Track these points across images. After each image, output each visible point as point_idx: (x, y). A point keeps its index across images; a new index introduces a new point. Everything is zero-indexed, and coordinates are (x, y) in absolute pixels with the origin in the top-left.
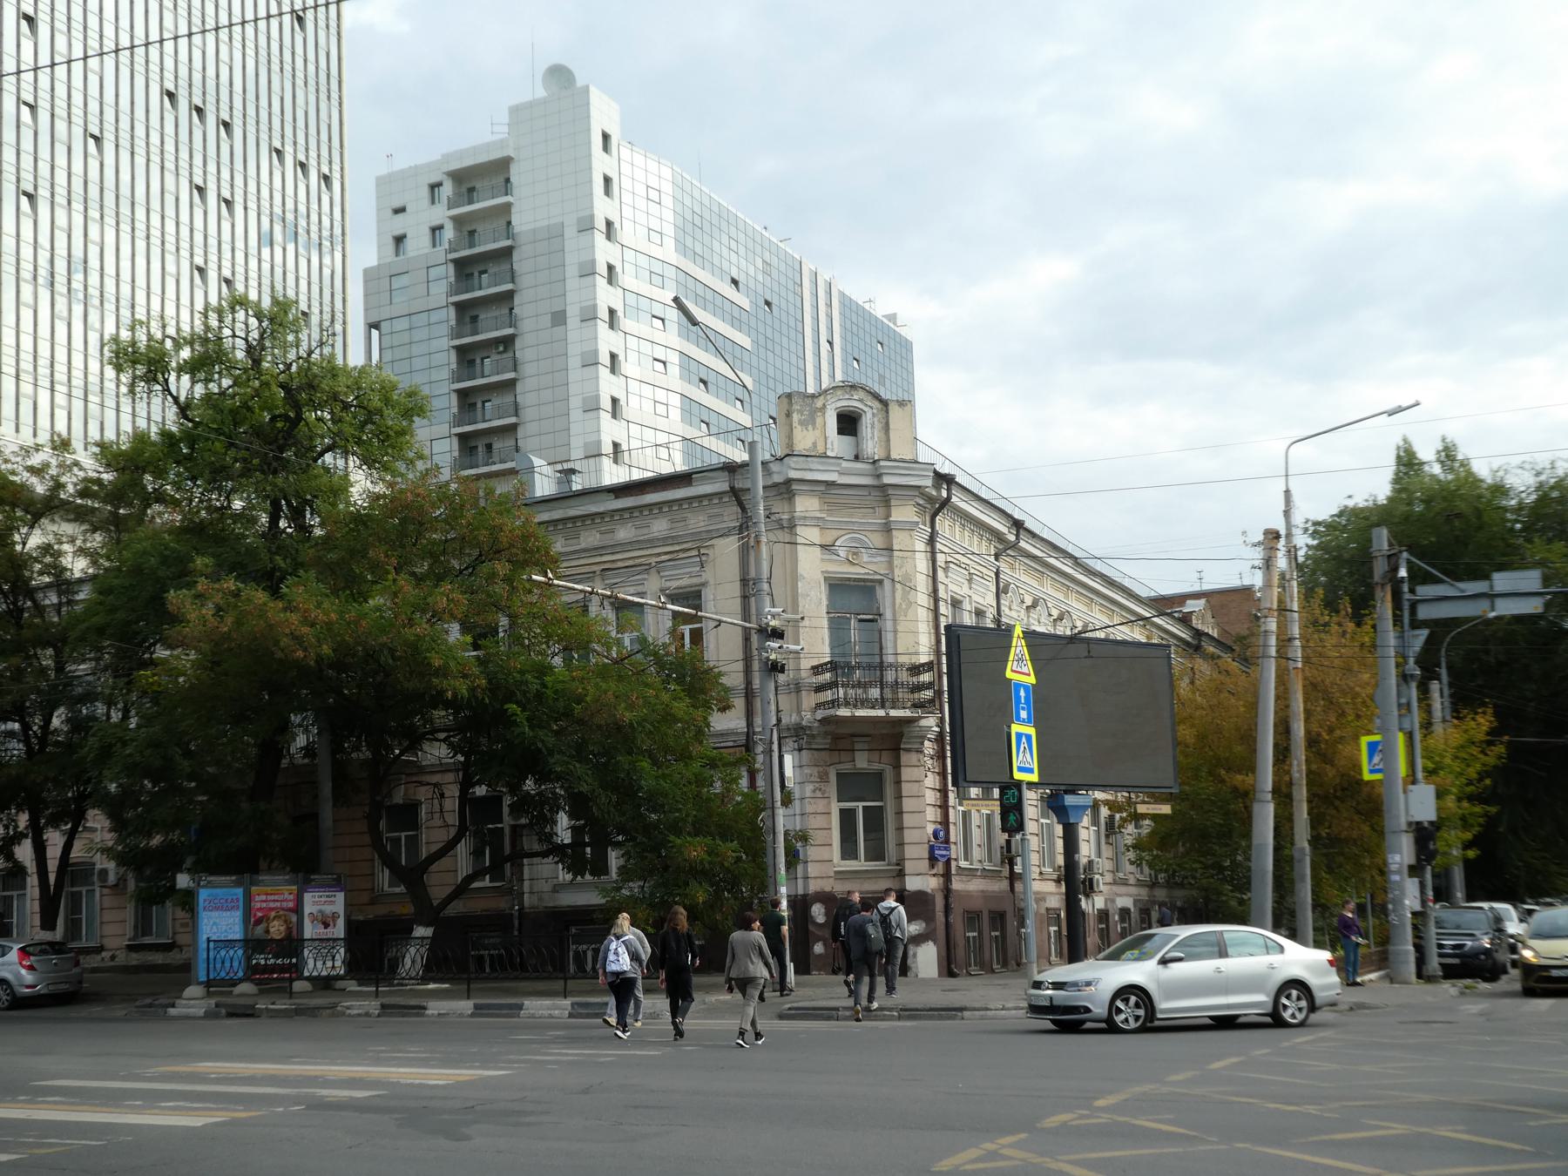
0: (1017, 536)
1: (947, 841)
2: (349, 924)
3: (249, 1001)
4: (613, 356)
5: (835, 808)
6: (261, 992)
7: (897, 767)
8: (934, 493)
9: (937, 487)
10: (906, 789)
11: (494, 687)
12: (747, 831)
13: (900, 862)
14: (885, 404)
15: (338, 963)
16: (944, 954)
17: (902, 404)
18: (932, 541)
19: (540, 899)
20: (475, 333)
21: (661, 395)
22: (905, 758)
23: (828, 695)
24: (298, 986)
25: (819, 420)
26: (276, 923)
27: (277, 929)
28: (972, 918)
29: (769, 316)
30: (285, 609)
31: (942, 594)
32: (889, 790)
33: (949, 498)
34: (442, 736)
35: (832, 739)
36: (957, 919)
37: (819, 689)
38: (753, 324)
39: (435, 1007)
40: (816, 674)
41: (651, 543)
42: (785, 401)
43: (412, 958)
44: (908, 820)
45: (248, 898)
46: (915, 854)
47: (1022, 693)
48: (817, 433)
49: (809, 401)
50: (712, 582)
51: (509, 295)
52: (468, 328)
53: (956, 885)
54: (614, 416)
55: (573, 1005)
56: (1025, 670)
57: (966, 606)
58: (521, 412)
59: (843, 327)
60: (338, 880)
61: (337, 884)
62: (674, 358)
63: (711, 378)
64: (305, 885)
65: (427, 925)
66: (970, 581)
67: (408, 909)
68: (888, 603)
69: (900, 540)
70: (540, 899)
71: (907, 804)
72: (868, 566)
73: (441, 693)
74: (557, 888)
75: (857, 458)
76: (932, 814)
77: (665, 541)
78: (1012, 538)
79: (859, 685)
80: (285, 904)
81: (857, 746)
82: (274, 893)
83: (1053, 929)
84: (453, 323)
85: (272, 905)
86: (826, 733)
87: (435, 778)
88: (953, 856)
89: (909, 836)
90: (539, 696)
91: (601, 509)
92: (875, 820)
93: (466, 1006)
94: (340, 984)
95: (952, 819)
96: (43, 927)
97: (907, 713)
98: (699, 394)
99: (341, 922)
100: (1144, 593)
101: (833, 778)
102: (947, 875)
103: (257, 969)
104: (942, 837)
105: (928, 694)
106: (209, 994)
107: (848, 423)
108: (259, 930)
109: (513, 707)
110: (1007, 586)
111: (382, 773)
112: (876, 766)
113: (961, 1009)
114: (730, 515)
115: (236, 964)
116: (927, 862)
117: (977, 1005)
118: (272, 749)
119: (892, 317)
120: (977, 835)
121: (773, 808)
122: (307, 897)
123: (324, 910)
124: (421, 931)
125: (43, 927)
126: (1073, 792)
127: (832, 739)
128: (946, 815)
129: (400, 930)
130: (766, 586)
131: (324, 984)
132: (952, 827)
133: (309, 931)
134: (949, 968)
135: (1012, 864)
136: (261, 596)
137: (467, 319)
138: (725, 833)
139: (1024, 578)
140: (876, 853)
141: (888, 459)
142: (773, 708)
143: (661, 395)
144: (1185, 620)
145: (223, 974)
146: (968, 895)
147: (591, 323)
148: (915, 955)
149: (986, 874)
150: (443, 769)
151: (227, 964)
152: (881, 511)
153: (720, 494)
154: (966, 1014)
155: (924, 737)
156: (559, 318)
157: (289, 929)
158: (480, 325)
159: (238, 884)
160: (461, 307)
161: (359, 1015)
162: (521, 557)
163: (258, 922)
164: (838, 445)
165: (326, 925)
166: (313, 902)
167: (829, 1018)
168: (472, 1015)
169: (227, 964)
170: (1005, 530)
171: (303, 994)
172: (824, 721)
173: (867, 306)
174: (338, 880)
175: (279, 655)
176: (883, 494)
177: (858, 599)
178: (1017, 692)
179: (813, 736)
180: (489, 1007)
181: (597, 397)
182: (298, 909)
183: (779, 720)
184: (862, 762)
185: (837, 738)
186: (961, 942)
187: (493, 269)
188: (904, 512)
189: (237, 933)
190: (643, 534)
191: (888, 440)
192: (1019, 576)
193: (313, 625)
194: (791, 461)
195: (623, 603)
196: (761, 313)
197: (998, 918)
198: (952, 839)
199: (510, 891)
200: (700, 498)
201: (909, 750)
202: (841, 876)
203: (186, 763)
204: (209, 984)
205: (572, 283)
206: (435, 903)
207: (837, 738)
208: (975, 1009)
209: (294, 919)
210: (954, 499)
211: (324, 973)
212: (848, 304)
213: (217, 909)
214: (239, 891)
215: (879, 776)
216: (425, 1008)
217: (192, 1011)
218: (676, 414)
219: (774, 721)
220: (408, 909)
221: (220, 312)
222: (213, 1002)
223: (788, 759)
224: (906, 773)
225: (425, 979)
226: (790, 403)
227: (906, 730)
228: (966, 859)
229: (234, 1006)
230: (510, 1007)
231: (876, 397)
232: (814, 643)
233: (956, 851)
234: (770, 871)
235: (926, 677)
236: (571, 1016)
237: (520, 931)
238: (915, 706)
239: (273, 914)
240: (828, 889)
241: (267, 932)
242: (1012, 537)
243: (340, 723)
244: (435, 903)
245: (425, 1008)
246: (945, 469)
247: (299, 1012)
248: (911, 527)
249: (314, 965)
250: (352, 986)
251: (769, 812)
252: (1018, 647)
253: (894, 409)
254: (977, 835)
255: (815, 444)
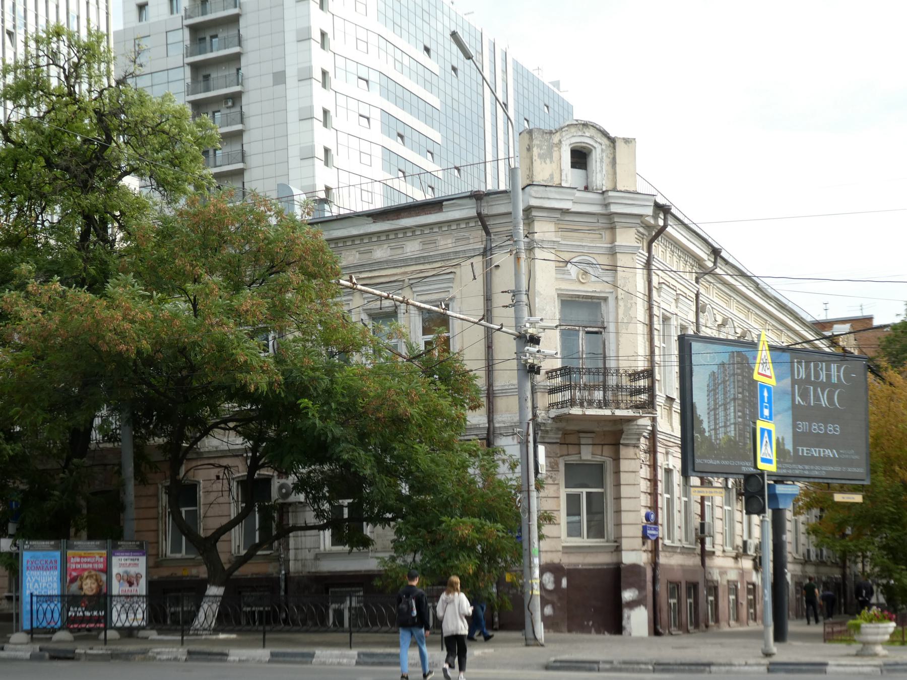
0: (715, 263)
1: (656, 523)
2: (151, 584)
3: (69, 647)
4: (326, 112)
5: (563, 492)
6: (76, 639)
7: (617, 459)
8: (652, 222)
9: (655, 217)
10: (624, 478)
11: (289, 384)
12: (505, 513)
13: (618, 540)
14: (613, 141)
15: (140, 616)
16: (652, 617)
17: (627, 141)
18: (648, 265)
19: (304, 566)
20: (207, 89)
21: (365, 147)
22: (623, 452)
23: (558, 397)
24: (112, 634)
25: (555, 155)
26: (88, 581)
27: (89, 587)
28: (674, 587)
29: (455, 80)
30: (108, 308)
31: (656, 311)
32: (609, 479)
33: (665, 226)
34: (231, 425)
35: (566, 434)
36: (662, 588)
37: (552, 391)
38: (442, 86)
39: (236, 654)
40: (549, 378)
41: (405, 262)
42: (526, 136)
43: (207, 612)
44: (625, 504)
45: (65, 560)
46: (631, 532)
47: (766, 394)
48: (554, 165)
49: (547, 137)
50: (458, 296)
51: (237, 57)
52: (201, 85)
53: (663, 560)
54: (326, 163)
55: (359, 655)
56: (768, 373)
57: (674, 322)
58: (247, 159)
59: (516, 91)
60: (141, 546)
61: (140, 549)
62: (375, 115)
63: (407, 133)
64: (114, 550)
65: (219, 585)
66: (677, 300)
67: (202, 572)
68: (612, 318)
69: (622, 260)
70: (304, 566)
71: (625, 491)
72: (592, 287)
73: (244, 386)
74: (318, 557)
75: (586, 188)
76: (645, 500)
77: (418, 261)
78: (710, 264)
79: (586, 387)
80: (96, 566)
81: (583, 441)
82: (86, 555)
83: (732, 597)
84: (189, 80)
85: (85, 566)
86: (558, 429)
87: (225, 462)
88: (660, 536)
89: (625, 518)
90: (328, 392)
91: (362, 232)
92: (596, 506)
93: (263, 654)
94: (142, 633)
95: (660, 505)
96: (570, 534)
97: (630, 413)
98: (396, 146)
99: (143, 582)
100: (809, 319)
101: (562, 468)
102: (655, 552)
103: (74, 620)
104: (652, 520)
105: (644, 397)
106: (33, 640)
107: (580, 158)
108: (74, 588)
109: (305, 402)
110: (705, 306)
111: (177, 455)
112: (599, 459)
113: (709, 665)
114: (476, 239)
115: (56, 615)
116: (640, 541)
117: (721, 661)
118: (80, 436)
119: (557, 84)
120: (678, 519)
121: (529, 491)
122: (115, 560)
123: (128, 570)
124: (214, 591)
125: (570, 534)
126: (782, 482)
127: (566, 434)
128: (655, 501)
129: (197, 590)
130: (524, 298)
131: (128, 633)
132: (660, 511)
133: (117, 588)
134: (655, 631)
135: (703, 543)
136: (86, 296)
137: (201, 78)
138: (490, 514)
139: (716, 300)
140: (597, 529)
141: (615, 189)
142: (529, 404)
143: (365, 147)
144: (833, 341)
145: (44, 624)
146: (670, 568)
147: (308, 82)
148: (629, 618)
149: (685, 551)
150: (234, 454)
151: (49, 615)
152: (607, 235)
153: (467, 220)
154: (713, 668)
155: (640, 435)
156: (280, 78)
157: (99, 587)
158: (212, 83)
159: (56, 548)
160: (195, 67)
161: (168, 660)
162: (312, 269)
163: (73, 580)
164: (572, 177)
165: (131, 584)
166: (120, 564)
167: (591, 670)
168: (269, 661)
169: (49, 615)
170: (705, 256)
171: (114, 641)
172: (557, 419)
173: (536, 73)
174: (141, 546)
175: (105, 348)
176: (609, 221)
177: (586, 314)
178: (762, 392)
179: (547, 432)
180: (284, 655)
181: (312, 148)
182: (107, 570)
183: (535, 416)
184: (587, 454)
185: (566, 433)
186: (664, 607)
187: (222, 34)
188: (627, 238)
189: (54, 589)
190: (398, 255)
191: (615, 173)
192: (711, 295)
193: (132, 322)
194: (532, 190)
195: (377, 315)
196: (448, 77)
197: (693, 587)
198: (660, 521)
199: (278, 558)
200: (449, 223)
201: (627, 445)
202: (567, 550)
203: (8, 447)
204: (31, 632)
205: (291, 46)
206: (226, 567)
207: (566, 433)
208: (720, 665)
209: (104, 578)
210: (669, 229)
211: (127, 624)
212: (520, 71)
213: (38, 568)
214: (57, 554)
215: (601, 467)
216: (227, 655)
217: (20, 654)
218: (378, 162)
219: (530, 416)
220: (202, 572)
221: (37, 41)
222: (37, 647)
223: (541, 449)
224: (624, 465)
225: (216, 631)
226: (531, 138)
227: (625, 428)
228: (669, 538)
229: (55, 650)
230: (303, 655)
231: (605, 134)
232: (550, 351)
233: (662, 531)
234: (525, 545)
235: (643, 383)
236: (358, 663)
237: (286, 591)
238: (637, 407)
239: (86, 574)
240: (556, 561)
241: (81, 588)
242: (711, 263)
243: (143, 413)
244: (226, 567)
245: (227, 655)
246: (661, 201)
247: (114, 656)
248: (633, 251)
249: (119, 617)
250: (153, 635)
251: (526, 494)
252: (763, 354)
253: (620, 146)
254: (678, 519)
255: (552, 176)
